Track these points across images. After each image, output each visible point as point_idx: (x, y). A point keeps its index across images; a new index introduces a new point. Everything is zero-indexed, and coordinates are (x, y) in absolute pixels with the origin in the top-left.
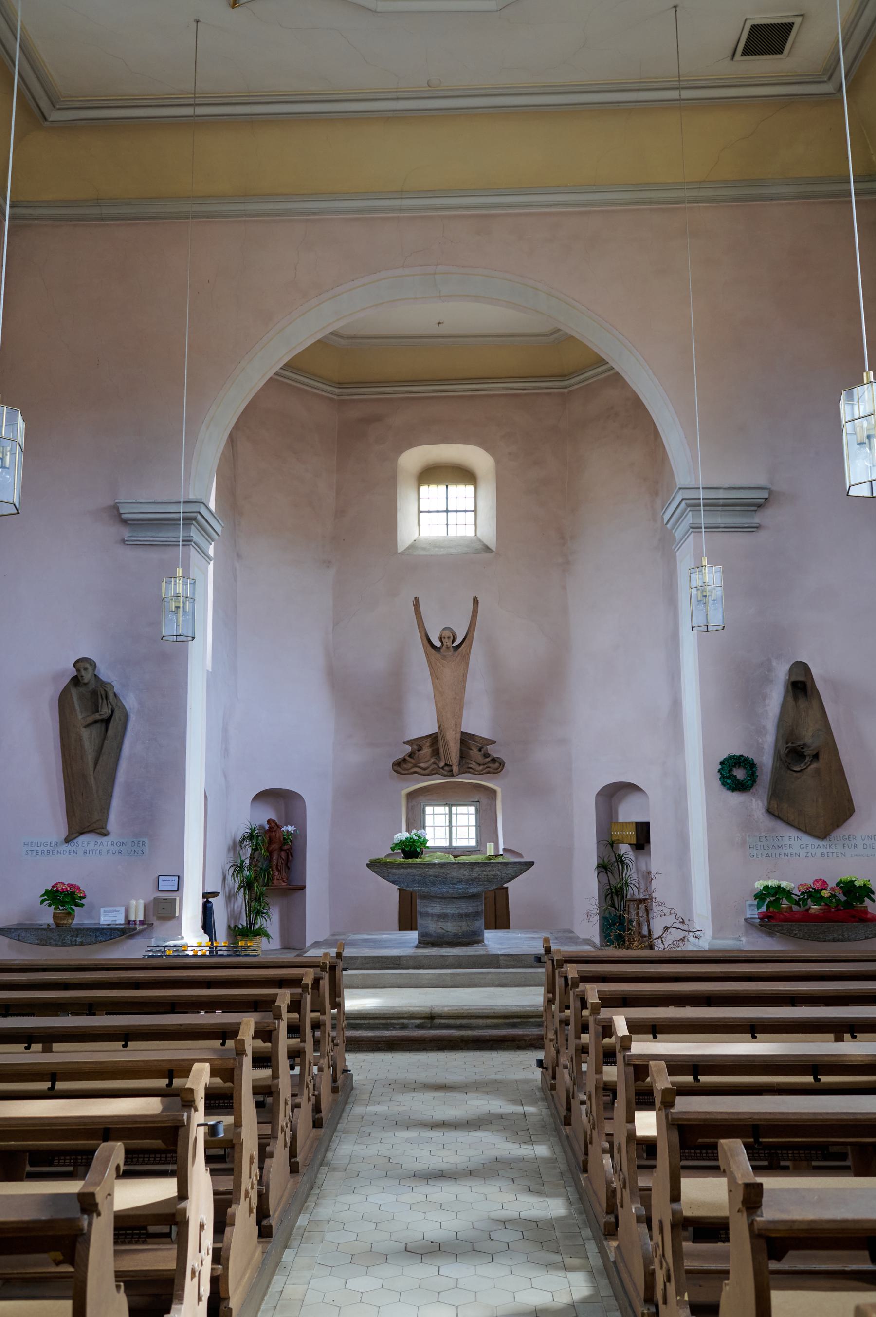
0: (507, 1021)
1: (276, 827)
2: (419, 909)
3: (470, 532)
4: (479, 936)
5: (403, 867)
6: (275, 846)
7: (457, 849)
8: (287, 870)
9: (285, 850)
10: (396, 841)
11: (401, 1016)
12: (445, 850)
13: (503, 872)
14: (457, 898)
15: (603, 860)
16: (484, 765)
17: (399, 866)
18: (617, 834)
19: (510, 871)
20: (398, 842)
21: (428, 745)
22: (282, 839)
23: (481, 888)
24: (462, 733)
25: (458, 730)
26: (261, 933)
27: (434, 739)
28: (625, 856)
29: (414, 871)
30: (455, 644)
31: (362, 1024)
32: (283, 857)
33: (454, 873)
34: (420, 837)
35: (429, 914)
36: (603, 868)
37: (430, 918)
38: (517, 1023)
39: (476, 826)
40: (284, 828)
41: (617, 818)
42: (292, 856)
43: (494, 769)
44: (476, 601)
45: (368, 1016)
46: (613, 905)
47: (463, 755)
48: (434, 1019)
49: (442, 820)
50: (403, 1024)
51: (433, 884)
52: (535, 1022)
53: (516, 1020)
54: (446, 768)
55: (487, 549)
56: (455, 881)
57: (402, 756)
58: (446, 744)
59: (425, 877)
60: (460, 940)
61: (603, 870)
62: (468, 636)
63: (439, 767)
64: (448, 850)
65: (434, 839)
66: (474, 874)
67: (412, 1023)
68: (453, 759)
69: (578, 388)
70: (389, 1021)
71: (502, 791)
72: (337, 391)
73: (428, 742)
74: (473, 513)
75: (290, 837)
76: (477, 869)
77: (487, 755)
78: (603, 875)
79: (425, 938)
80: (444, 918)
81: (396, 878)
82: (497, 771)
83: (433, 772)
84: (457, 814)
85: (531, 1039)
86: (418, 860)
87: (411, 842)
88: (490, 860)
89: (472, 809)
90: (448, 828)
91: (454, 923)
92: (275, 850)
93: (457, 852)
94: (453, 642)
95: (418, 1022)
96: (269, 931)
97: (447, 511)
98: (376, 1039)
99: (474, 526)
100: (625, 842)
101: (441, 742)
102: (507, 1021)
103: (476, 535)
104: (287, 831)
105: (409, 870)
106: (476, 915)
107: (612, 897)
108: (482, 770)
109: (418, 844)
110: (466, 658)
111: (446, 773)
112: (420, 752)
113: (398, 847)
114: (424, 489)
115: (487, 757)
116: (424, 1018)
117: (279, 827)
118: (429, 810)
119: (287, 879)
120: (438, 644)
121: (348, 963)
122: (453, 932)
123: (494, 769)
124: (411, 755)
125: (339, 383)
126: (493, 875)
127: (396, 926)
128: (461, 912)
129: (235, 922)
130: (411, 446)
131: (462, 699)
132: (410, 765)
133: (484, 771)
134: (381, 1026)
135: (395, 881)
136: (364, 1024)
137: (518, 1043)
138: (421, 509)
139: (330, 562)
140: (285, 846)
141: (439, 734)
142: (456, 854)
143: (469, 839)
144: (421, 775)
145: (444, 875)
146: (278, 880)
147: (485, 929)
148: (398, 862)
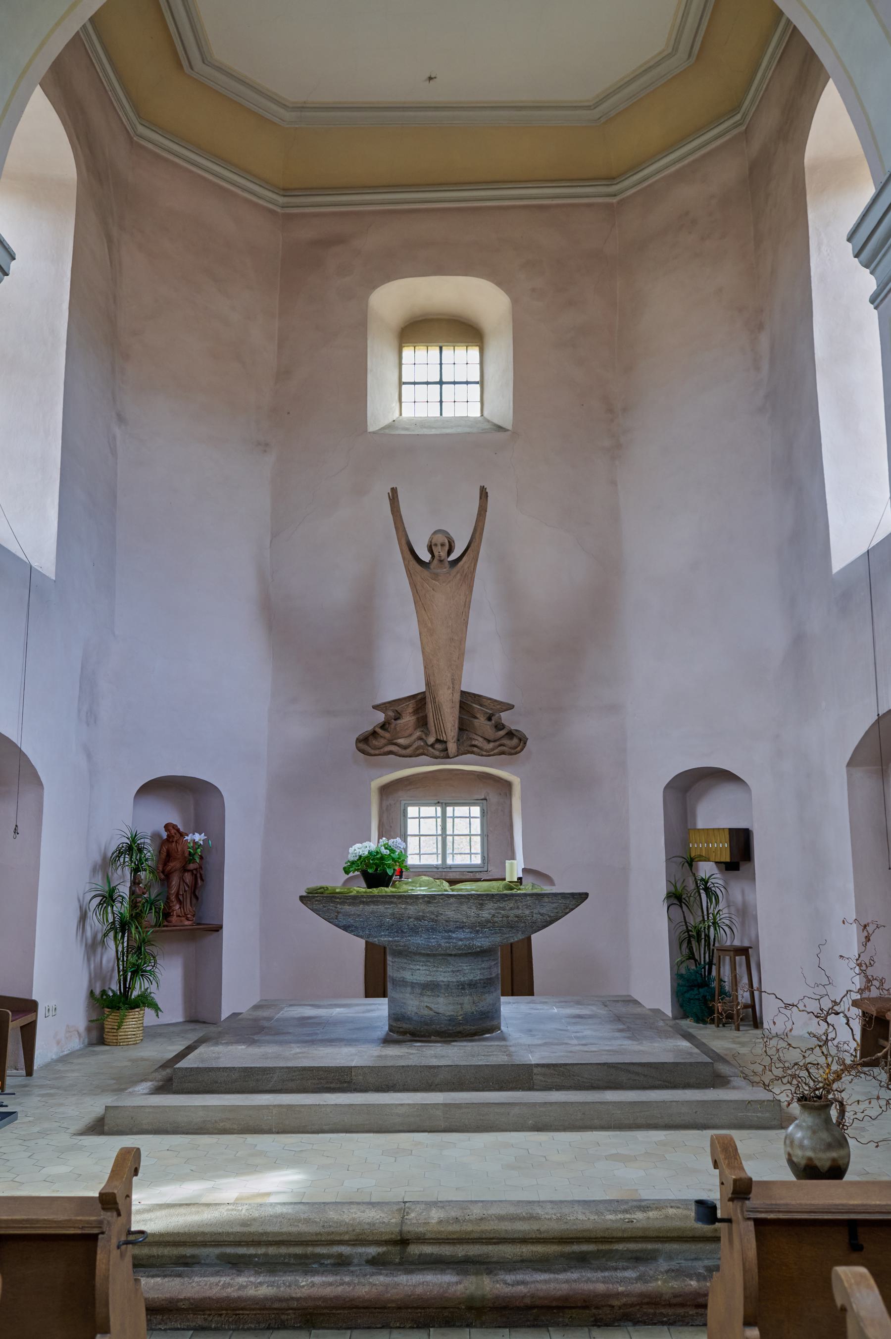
0: (568, 1249)
1: (178, 835)
2: (390, 972)
3: (475, 412)
4: (493, 1018)
5: (363, 903)
6: (175, 864)
7: (453, 870)
8: (194, 901)
9: (191, 871)
10: (351, 858)
11: (338, 1238)
12: (435, 870)
13: (535, 911)
14: (455, 955)
15: (675, 887)
16: (495, 741)
17: (356, 900)
18: (697, 846)
19: (547, 908)
20: (356, 859)
21: (410, 710)
22: (187, 854)
23: (497, 939)
24: (462, 692)
25: (457, 687)
26: (145, 1001)
27: (420, 702)
28: (713, 881)
29: (381, 908)
30: (453, 557)
31: (251, 1256)
32: (187, 881)
33: (450, 913)
34: (392, 851)
35: (407, 982)
36: (676, 898)
37: (409, 989)
38: (587, 1253)
39: (482, 835)
40: (189, 838)
41: (695, 824)
42: (202, 880)
43: (511, 748)
44: (484, 494)
45: (264, 1238)
46: (691, 956)
47: (464, 727)
48: (408, 1244)
49: (431, 827)
50: (340, 1255)
51: (414, 931)
52: (628, 1250)
53: (585, 1248)
54: (438, 746)
55: (500, 428)
56: (452, 926)
57: (369, 728)
58: (438, 709)
59: (400, 920)
60: (460, 1028)
61: (676, 902)
62: (472, 545)
63: (425, 742)
64: (440, 870)
65: (419, 854)
66: (485, 914)
67: (361, 1255)
68: (449, 731)
69: (634, 193)
70: (310, 1250)
71: (522, 782)
72: (281, 200)
73: (411, 707)
74: (478, 386)
75: (199, 850)
76: (490, 905)
77: (499, 726)
78: (676, 909)
79: (399, 1024)
80: (432, 990)
81: (351, 921)
82: (514, 751)
83: (418, 752)
84: (453, 817)
85: (624, 1305)
86: (389, 890)
87: (378, 859)
88: (512, 889)
89: (476, 811)
90: (440, 838)
91: (451, 998)
92: (175, 871)
93: (454, 874)
94: (450, 552)
95: (373, 1251)
96: (158, 997)
97: (441, 383)
98: (276, 1305)
99: (479, 404)
100: (711, 859)
101: (429, 706)
102: (568, 1249)
103: (482, 415)
104: (195, 843)
105: (372, 907)
106: (487, 984)
107: (689, 942)
108: (493, 750)
109: (390, 862)
110: (468, 579)
111: (437, 753)
112: (399, 722)
113: (354, 867)
114: (408, 353)
115: (501, 730)
116: (387, 1243)
117: (182, 835)
118: (412, 811)
119: (194, 916)
120: (425, 557)
121: (257, 1080)
122: (449, 1013)
123: (511, 748)
124: (383, 726)
125: (284, 189)
126: (517, 916)
127: (361, 987)
128: (462, 979)
129: (103, 983)
130: (389, 277)
131: (462, 640)
132: (383, 741)
133: (495, 751)
134: (292, 1261)
135: (349, 927)
136: (256, 1256)
137: (594, 1311)
138: (404, 380)
139: (267, 445)
140: (191, 865)
141: (427, 694)
142: (452, 876)
143: (471, 854)
144: (400, 756)
145: (433, 917)
146: (179, 916)
147: (503, 995)
148: (354, 893)
